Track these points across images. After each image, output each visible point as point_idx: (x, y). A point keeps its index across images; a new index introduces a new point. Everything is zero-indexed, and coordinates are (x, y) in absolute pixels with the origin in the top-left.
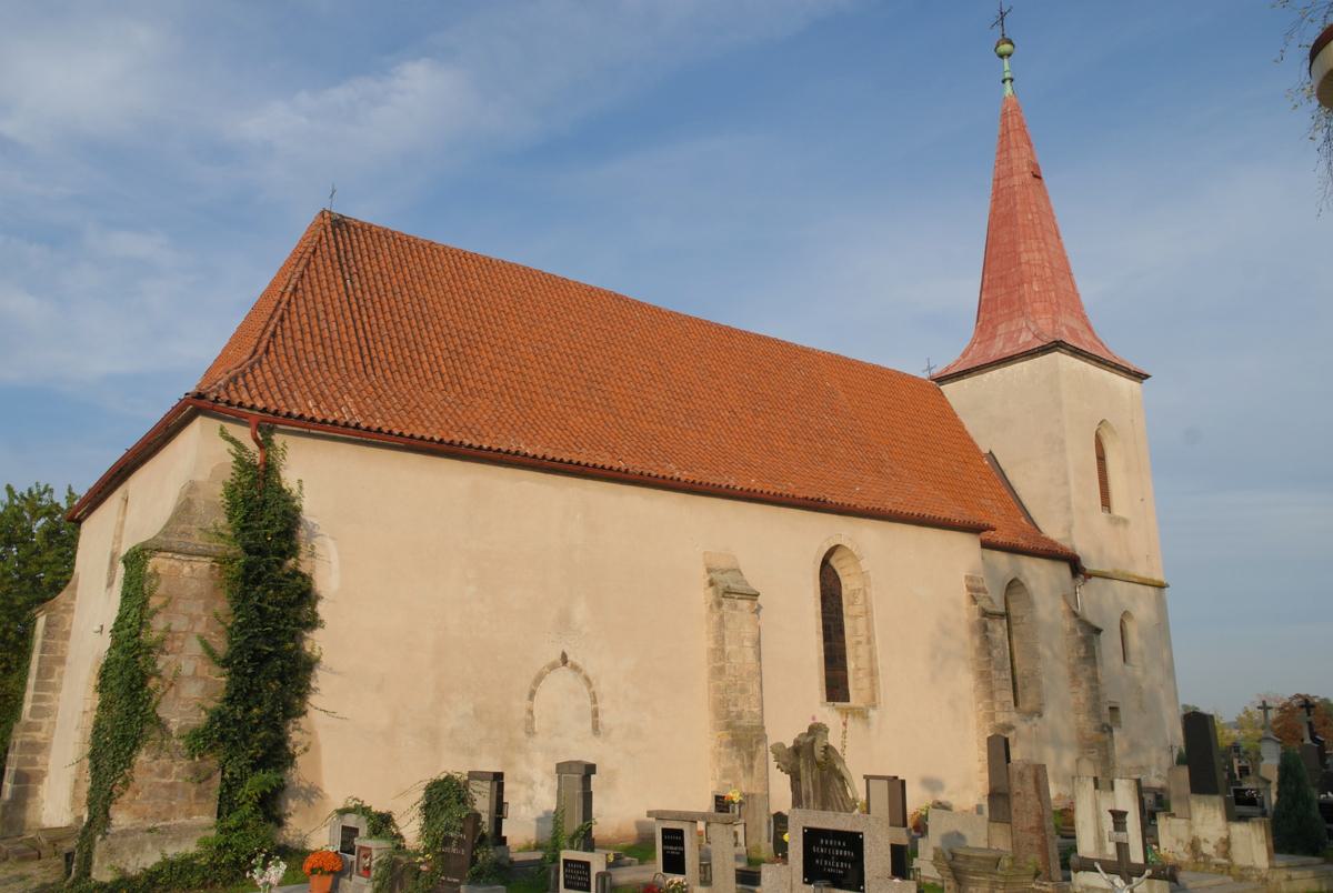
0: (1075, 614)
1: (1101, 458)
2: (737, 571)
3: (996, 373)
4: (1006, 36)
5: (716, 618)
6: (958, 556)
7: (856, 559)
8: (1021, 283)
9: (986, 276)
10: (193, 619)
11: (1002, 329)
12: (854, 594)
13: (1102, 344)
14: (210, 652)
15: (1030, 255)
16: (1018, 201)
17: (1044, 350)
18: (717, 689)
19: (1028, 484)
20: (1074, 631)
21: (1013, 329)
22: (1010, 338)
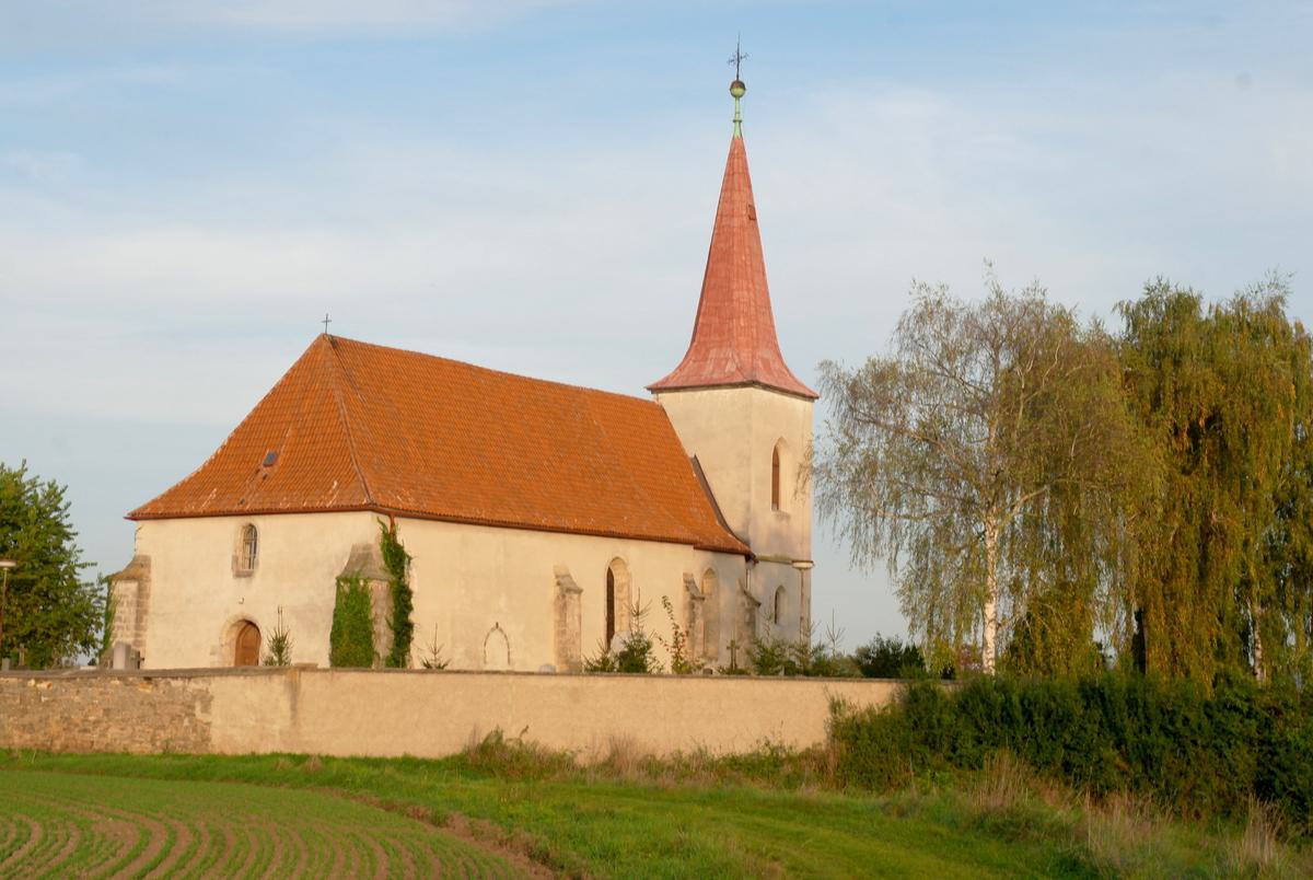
0: (745, 593)
1: (776, 466)
2: (569, 576)
3: (705, 393)
4: (740, 79)
5: (561, 603)
6: (687, 561)
7: (625, 565)
8: (731, 319)
9: (704, 303)
10: (383, 609)
11: (713, 353)
12: (622, 586)
13: (788, 370)
14: (389, 624)
15: (741, 294)
16: (736, 242)
17: (744, 385)
18: (560, 642)
19: (724, 487)
20: (743, 604)
21: (722, 356)
22: (719, 365)
